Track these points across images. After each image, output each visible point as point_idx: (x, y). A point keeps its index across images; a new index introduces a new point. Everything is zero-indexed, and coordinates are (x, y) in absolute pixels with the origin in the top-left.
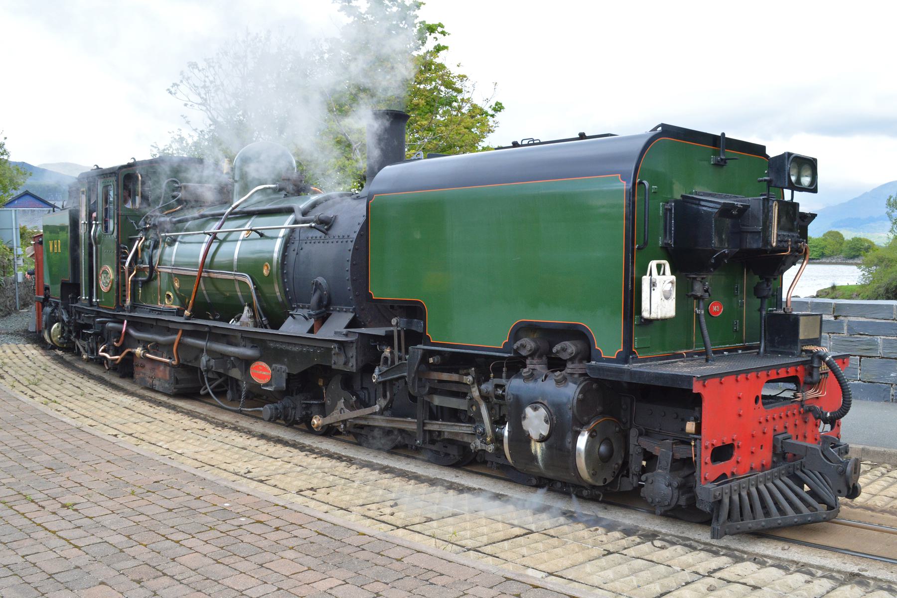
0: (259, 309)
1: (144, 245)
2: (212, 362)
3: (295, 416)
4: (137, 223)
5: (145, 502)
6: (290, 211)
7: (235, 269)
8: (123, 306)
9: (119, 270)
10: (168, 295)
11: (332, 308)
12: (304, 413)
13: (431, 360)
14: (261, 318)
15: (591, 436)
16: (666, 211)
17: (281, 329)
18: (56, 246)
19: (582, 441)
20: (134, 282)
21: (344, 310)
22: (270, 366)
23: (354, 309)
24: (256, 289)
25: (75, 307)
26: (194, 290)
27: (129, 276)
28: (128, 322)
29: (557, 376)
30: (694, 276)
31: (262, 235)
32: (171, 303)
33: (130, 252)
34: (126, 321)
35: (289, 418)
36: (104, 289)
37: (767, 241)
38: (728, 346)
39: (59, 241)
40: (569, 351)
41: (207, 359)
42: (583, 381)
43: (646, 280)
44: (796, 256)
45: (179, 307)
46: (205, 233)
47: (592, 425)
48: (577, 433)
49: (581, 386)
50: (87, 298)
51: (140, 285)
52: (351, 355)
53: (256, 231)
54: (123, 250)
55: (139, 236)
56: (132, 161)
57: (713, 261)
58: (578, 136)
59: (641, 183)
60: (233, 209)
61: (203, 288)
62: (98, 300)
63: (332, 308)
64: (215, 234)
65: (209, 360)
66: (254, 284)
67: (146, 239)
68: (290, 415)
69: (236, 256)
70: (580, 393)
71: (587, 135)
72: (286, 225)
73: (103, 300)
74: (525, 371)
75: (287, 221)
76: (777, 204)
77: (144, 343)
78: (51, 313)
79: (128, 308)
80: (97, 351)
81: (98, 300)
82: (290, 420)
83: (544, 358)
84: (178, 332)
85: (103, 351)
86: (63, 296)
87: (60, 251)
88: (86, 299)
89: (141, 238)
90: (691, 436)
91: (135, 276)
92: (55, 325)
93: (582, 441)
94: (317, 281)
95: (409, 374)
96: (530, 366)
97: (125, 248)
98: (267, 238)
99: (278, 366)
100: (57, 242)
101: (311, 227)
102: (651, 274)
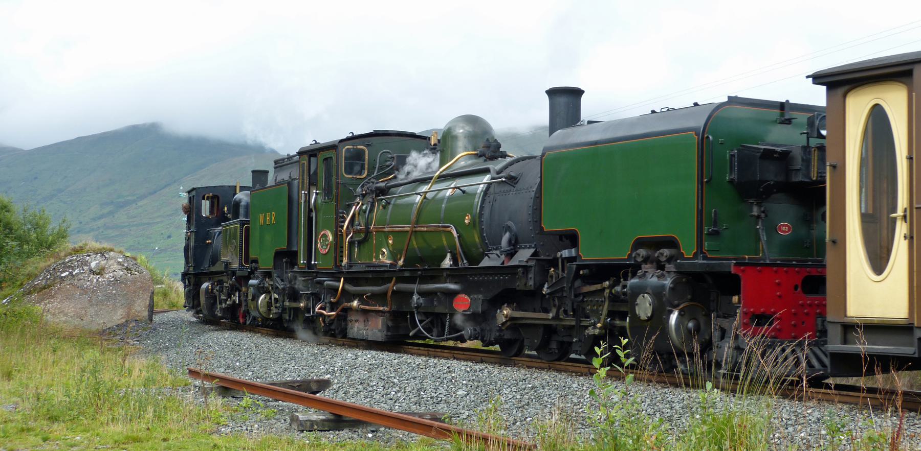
0: (461, 253)
1: (360, 210)
2: (421, 300)
3: (490, 337)
4: (355, 190)
6: (486, 171)
8: (341, 265)
9: (338, 236)
10: (382, 251)
11: (518, 246)
12: (498, 334)
13: (581, 272)
14: (463, 261)
15: (679, 314)
16: (732, 156)
19: (674, 317)
20: (351, 243)
21: (528, 246)
22: (469, 296)
23: (535, 245)
24: (459, 237)
26: (405, 248)
27: (347, 236)
28: (344, 279)
29: (658, 273)
30: (752, 201)
32: (385, 258)
33: (348, 216)
34: (342, 279)
35: (485, 339)
36: (323, 251)
37: (808, 175)
38: (791, 258)
40: (665, 254)
41: (417, 298)
42: (674, 277)
45: (391, 262)
46: (416, 194)
47: (681, 306)
48: (671, 312)
49: (673, 279)
50: (305, 262)
51: (356, 245)
52: (530, 276)
53: (458, 188)
54: (341, 215)
55: (356, 201)
56: (351, 135)
57: (761, 190)
58: (693, 105)
59: (708, 137)
60: (441, 172)
61: (415, 243)
62: (316, 263)
63: (518, 246)
65: (419, 299)
66: (457, 233)
67: (363, 204)
68: (486, 336)
70: (671, 284)
71: (700, 104)
72: (484, 181)
73: (321, 262)
74: (640, 273)
75: (486, 178)
77: (359, 296)
79: (345, 266)
80: (314, 309)
81: (316, 263)
82: (486, 340)
83: (655, 264)
84: (392, 280)
85: (319, 309)
87: (274, 222)
88: (304, 263)
89: (358, 203)
90: (736, 305)
91: (351, 237)
92: (263, 296)
93: (674, 317)
94: (507, 224)
96: (644, 270)
97: (343, 213)
99: (476, 296)
100: (271, 214)
101: (502, 181)
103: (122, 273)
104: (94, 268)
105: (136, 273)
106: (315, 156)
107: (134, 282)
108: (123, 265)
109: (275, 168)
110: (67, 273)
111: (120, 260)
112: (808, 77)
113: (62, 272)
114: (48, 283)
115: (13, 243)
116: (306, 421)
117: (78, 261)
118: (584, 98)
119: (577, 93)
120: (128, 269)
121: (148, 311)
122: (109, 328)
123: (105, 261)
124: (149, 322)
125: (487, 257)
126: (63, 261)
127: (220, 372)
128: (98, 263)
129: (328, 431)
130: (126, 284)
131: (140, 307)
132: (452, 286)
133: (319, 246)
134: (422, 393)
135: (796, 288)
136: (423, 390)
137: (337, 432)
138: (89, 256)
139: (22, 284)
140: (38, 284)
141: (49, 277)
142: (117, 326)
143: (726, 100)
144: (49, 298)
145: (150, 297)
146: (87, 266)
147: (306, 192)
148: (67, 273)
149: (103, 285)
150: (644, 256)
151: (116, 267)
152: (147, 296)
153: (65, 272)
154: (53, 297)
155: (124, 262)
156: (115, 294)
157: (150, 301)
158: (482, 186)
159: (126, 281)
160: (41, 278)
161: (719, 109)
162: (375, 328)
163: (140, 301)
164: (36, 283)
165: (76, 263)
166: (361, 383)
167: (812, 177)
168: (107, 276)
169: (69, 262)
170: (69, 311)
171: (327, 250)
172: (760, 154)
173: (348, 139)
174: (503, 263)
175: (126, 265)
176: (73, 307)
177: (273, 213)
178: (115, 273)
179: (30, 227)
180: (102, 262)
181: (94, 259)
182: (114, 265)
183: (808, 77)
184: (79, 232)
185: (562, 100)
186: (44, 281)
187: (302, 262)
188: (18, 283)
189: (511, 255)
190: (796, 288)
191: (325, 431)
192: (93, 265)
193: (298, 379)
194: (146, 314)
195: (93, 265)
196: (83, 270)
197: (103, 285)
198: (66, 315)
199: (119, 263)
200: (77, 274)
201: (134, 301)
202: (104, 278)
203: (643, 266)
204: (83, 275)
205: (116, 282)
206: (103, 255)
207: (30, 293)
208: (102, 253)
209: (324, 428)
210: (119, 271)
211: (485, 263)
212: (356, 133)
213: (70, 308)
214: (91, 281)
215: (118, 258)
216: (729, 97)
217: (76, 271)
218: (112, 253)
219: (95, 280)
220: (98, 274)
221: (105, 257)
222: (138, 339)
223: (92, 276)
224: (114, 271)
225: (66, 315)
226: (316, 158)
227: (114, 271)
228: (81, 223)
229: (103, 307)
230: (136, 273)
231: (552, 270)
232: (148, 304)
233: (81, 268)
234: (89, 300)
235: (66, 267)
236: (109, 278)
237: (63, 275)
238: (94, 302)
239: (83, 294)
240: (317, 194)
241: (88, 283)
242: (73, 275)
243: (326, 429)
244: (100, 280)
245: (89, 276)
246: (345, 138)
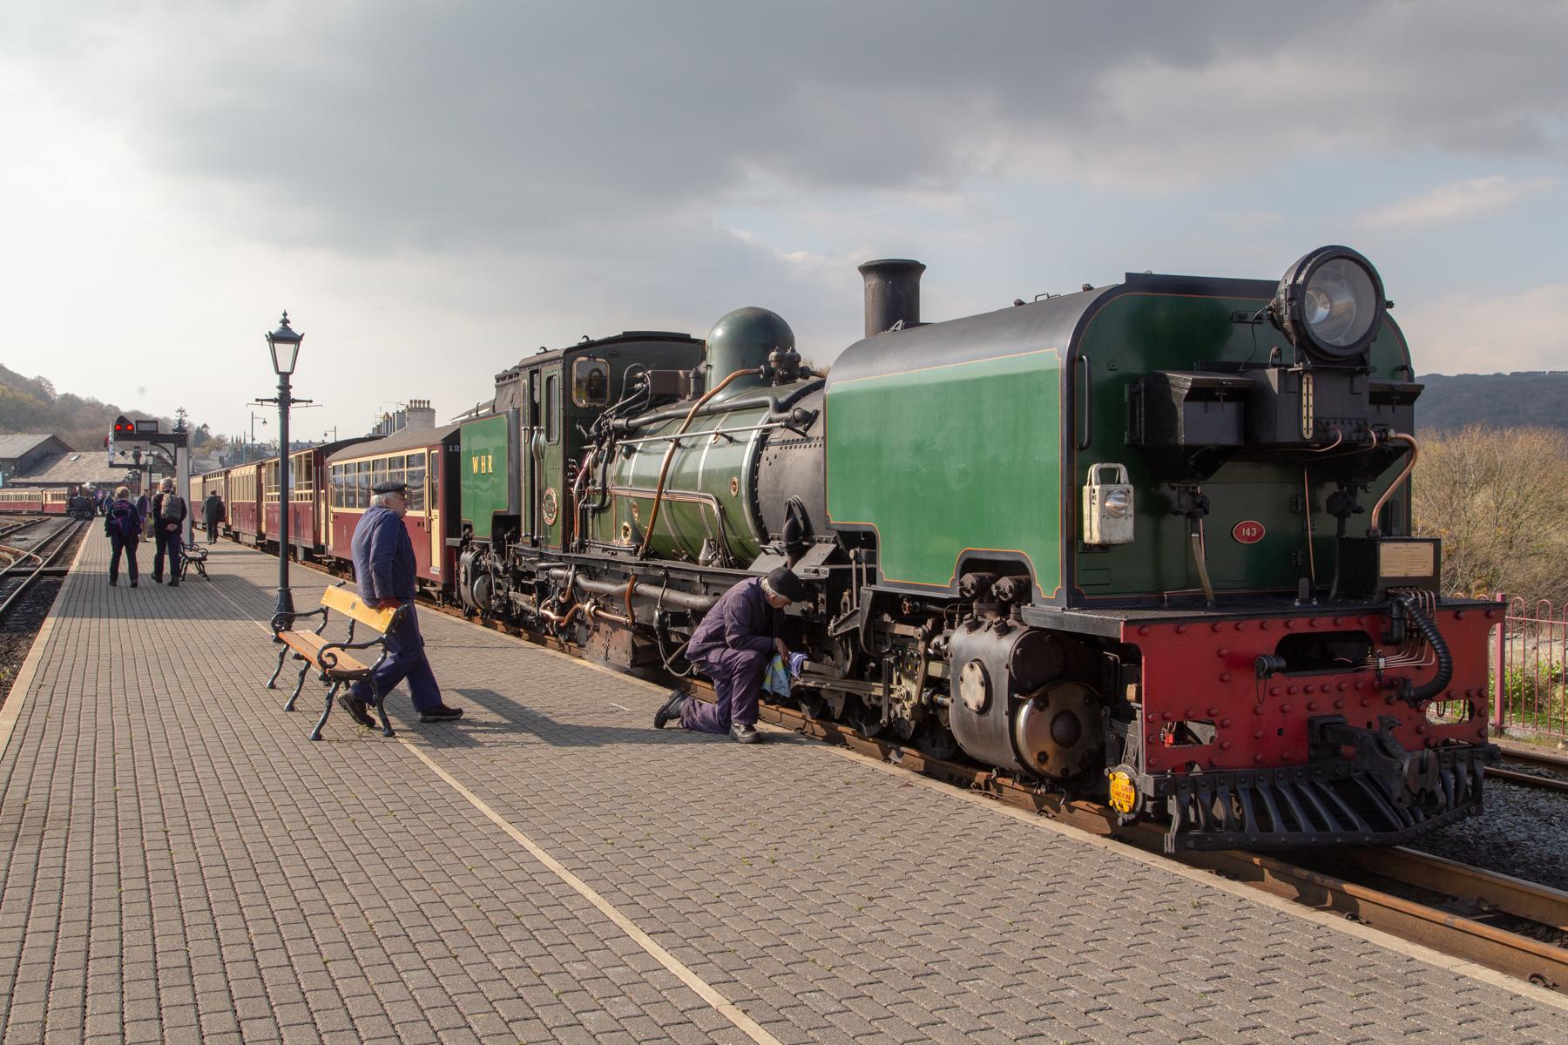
5: (415, 776)
7: (699, 488)
17: (750, 569)
18: (483, 464)
20: (584, 511)
25: (514, 548)
31: (731, 440)
39: (490, 457)
43: (1086, 488)
44: (31, 638)
56: (585, 340)
64: (678, 440)
69: (701, 469)
72: (759, 425)
76: (1310, 377)
78: (474, 562)
86: (497, 538)
87: (490, 470)
95: (861, 625)
98: (738, 442)
100: (487, 459)
102: (1090, 484)
109: (496, 387)
112: (303, 335)
118: (926, 283)
125: (763, 554)
127: (1208, 485)
133: (545, 516)
143: (1122, 281)
158: (756, 431)
161: (1099, 307)
171: (553, 520)
172: (1186, 392)
173: (581, 347)
177: (490, 457)
183: (303, 335)
212: (595, 337)
216: (1128, 275)
246: (576, 345)
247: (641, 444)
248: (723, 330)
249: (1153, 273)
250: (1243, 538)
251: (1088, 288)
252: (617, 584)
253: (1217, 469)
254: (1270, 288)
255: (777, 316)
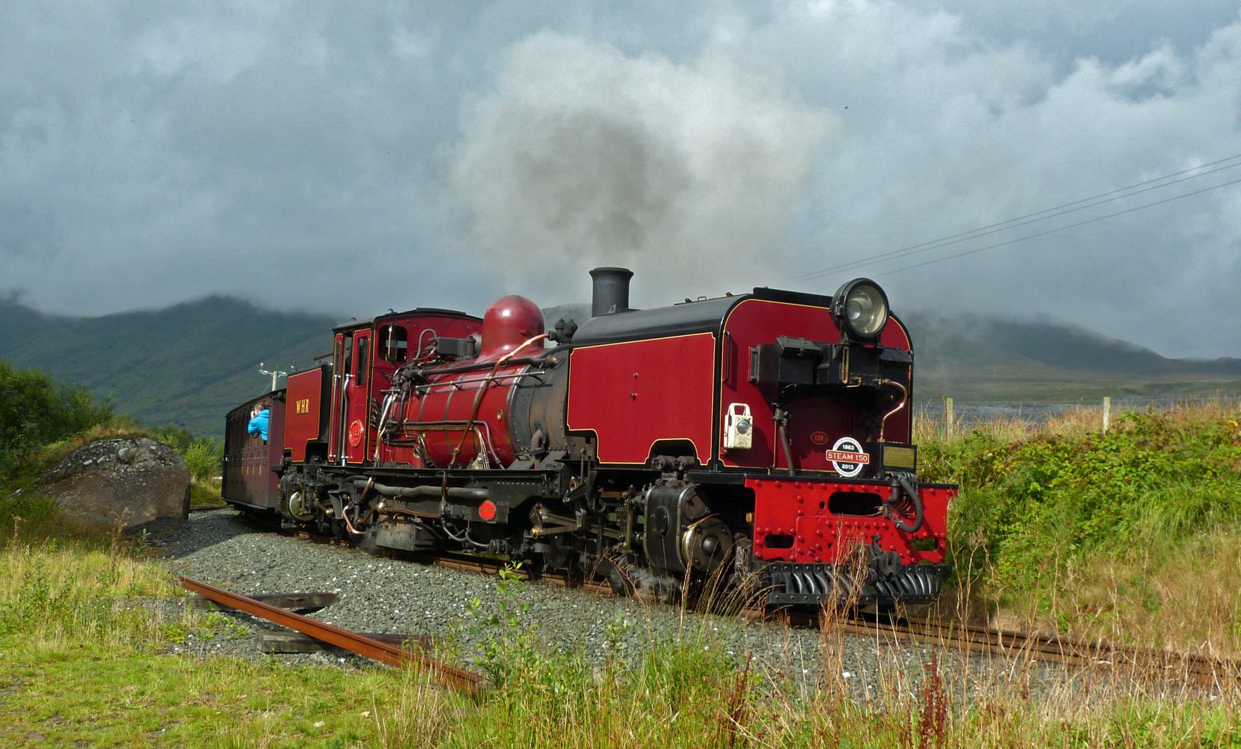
12: (527, 548)
19: (688, 535)
22: (495, 502)
56: (390, 312)
87: (307, 411)
103: (154, 462)
104: (122, 456)
105: (171, 463)
106: (350, 335)
107: (168, 473)
108: (156, 454)
110: (91, 461)
111: (153, 448)
113: (85, 460)
114: (68, 471)
115: (33, 425)
116: (272, 641)
117: (103, 448)
118: (633, 283)
119: (624, 276)
120: (161, 458)
121: (183, 508)
122: (136, 526)
123: (136, 449)
124: (183, 520)
125: (517, 460)
126: (87, 447)
128: (128, 450)
129: (298, 653)
130: (158, 476)
131: (174, 502)
132: (480, 493)
134: (427, 613)
135: (822, 505)
136: (429, 609)
137: (307, 655)
138: (117, 442)
139: (39, 472)
140: (56, 473)
141: (69, 465)
142: (145, 524)
144: (68, 490)
145: (186, 492)
146: (113, 453)
147: (339, 376)
148: (91, 461)
149: (131, 476)
150: (685, 465)
151: (147, 455)
152: (182, 490)
153: (88, 459)
154: (72, 488)
155: (157, 450)
156: (145, 487)
157: (185, 496)
159: (159, 472)
160: (61, 466)
162: (399, 535)
163: (173, 496)
164: (55, 472)
165: (102, 450)
166: (369, 599)
167: (843, 378)
168: (137, 466)
169: (93, 448)
170: (91, 505)
174: (533, 467)
175: (159, 453)
176: (95, 500)
177: (307, 400)
178: (146, 462)
179: (68, 405)
180: (132, 450)
181: (122, 445)
182: (145, 454)
184: (157, 411)
185: (607, 282)
186: (64, 469)
187: (331, 455)
188: (36, 471)
189: (541, 456)
190: (822, 505)
191: (294, 653)
192: (121, 452)
193: (306, 592)
194: (180, 510)
195: (121, 452)
196: (109, 458)
197: (131, 476)
198: (87, 509)
199: (152, 451)
200: (102, 463)
201: (167, 496)
202: (133, 468)
203: (663, 474)
204: (110, 464)
205: (147, 473)
206: (133, 442)
207: (47, 483)
208: (133, 438)
209: (294, 650)
210: (152, 461)
211: (516, 466)
213: (92, 501)
214: (118, 471)
215: (150, 445)
217: (101, 459)
218: (144, 440)
219: (123, 471)
220: (126, 463)
221: (136, 444)
222: (167, 540)
223: (119, 465)
224: (146, 460)
225: (87, 509)
226: (351, 338)
227: (146, 460)
228: (160, 401)
229: (131, 502)
230: (171, 463)
231: (573, 478)
232: (183, 499)
233: (107, 456)
234: (115, 493)
235: (90, 454)
236: (139, 468)
237: (86, 463)
238: (120, 495)
239: (107, 486)
240: (350, 378)
241: (114, 474)
242: (97, 464)
243: (296, 651)
244: (128, 470)
245: (115, 466)
247: (429, 389)
248: (512, 313)
249: (769, 288)
250: (817, 442)
251: (729, 295)
252: (420, 489)
253: (401, 349)
254: (826, 300)
255: (532, 303)
